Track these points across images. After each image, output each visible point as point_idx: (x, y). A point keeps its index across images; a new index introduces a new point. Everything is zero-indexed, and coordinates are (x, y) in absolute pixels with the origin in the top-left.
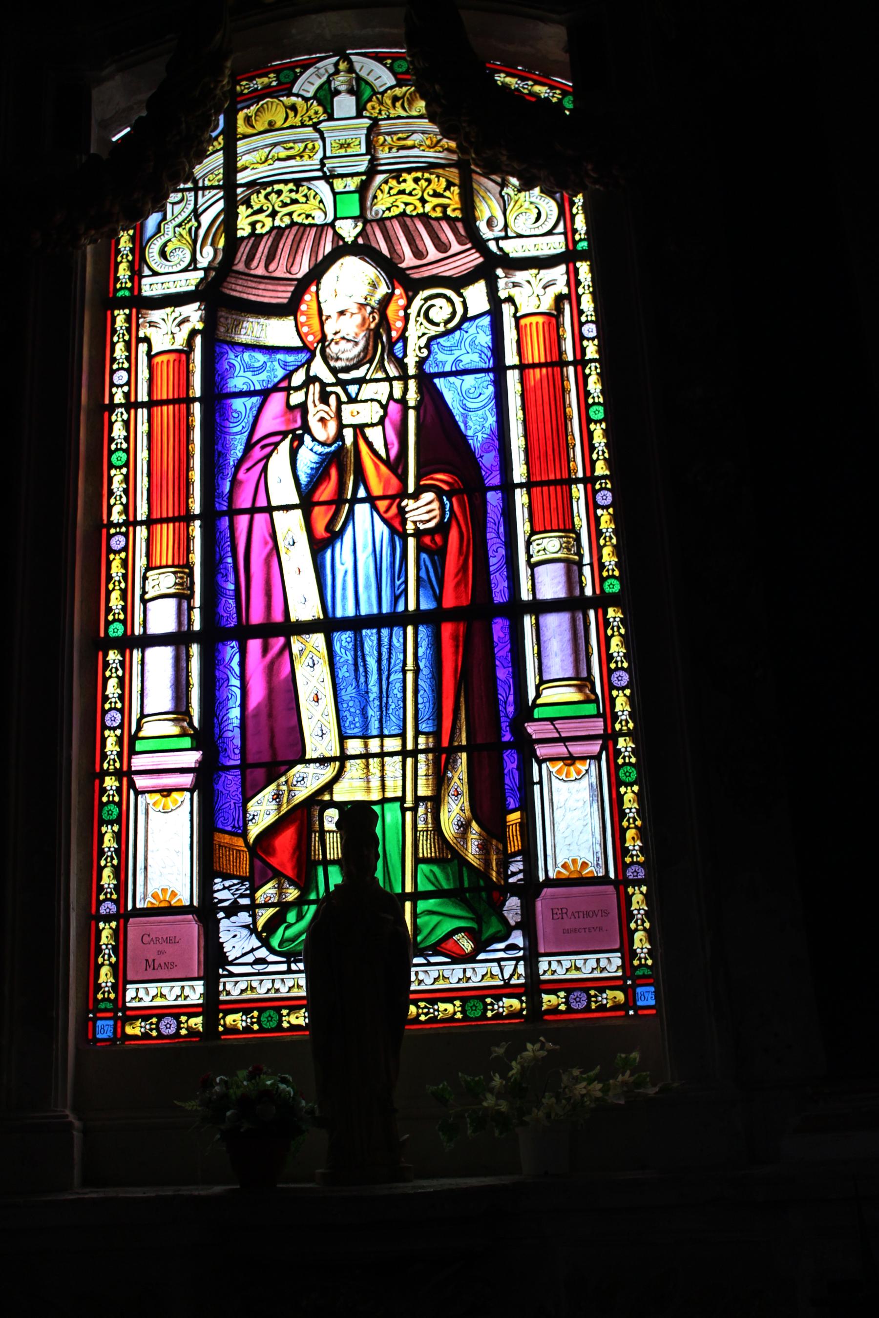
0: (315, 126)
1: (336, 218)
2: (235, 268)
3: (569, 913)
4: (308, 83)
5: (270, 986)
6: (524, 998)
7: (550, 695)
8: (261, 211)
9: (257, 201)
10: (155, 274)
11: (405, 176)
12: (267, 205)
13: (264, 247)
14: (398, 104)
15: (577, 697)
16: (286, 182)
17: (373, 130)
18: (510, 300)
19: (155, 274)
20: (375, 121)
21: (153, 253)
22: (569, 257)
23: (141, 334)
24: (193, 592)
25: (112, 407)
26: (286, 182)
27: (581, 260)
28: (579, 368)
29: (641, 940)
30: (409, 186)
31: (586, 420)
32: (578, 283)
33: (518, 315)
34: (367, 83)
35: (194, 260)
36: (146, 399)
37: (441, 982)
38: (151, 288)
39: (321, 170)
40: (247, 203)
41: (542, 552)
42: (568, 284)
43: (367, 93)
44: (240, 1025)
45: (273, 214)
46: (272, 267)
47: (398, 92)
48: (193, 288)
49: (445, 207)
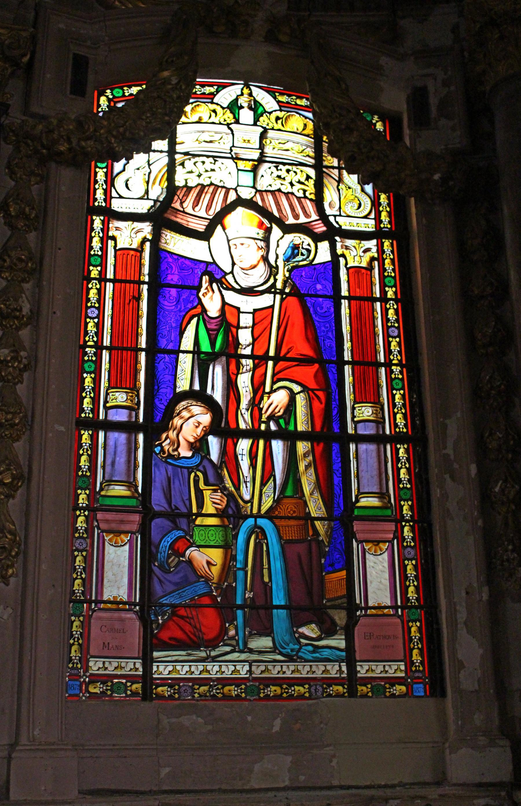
0: (228, 125)
1: (238, 186)
2: (173, 205)
3: (375, 636)
4: (225, 97)
5: (280, 669)
6: (346, 687)
7: (364, 502)
8: (191, 172)
9: (189, 165)
10: (121, 197)
11: (281, 167)
12: (194, 169)
13: (193, 194)
14: (279, 122)
15: (128, 493)
16: (208, 157)
17: (263, 136)
18: (343, 256)
19: (121, 197)
20: (265, 131)
21: (119, 183)
22: (378, 234)
23: (110, 234)
24: (385, 420)
25: (89, 279)
26: (208, 157)
27: (386, 239)
28: (383, 304)
29: (76, 651)
30: (283, 174)
31: (387, 336)
32: (383, 252)
33: (348, 266)
34: (261, 105)
35: (147, 192)
36: (112, 277)
37: (119, 670)
38: (117, 205)
39: (230, 153)
40: (182, 164)
41: (114, 401)
42: (378, 251)
43: (260, 110)
44: (234, 694)
45: (199, 176)
46: (197, 209)
47: (281, 114)
48: (146, 211)
49: (305, 191)
